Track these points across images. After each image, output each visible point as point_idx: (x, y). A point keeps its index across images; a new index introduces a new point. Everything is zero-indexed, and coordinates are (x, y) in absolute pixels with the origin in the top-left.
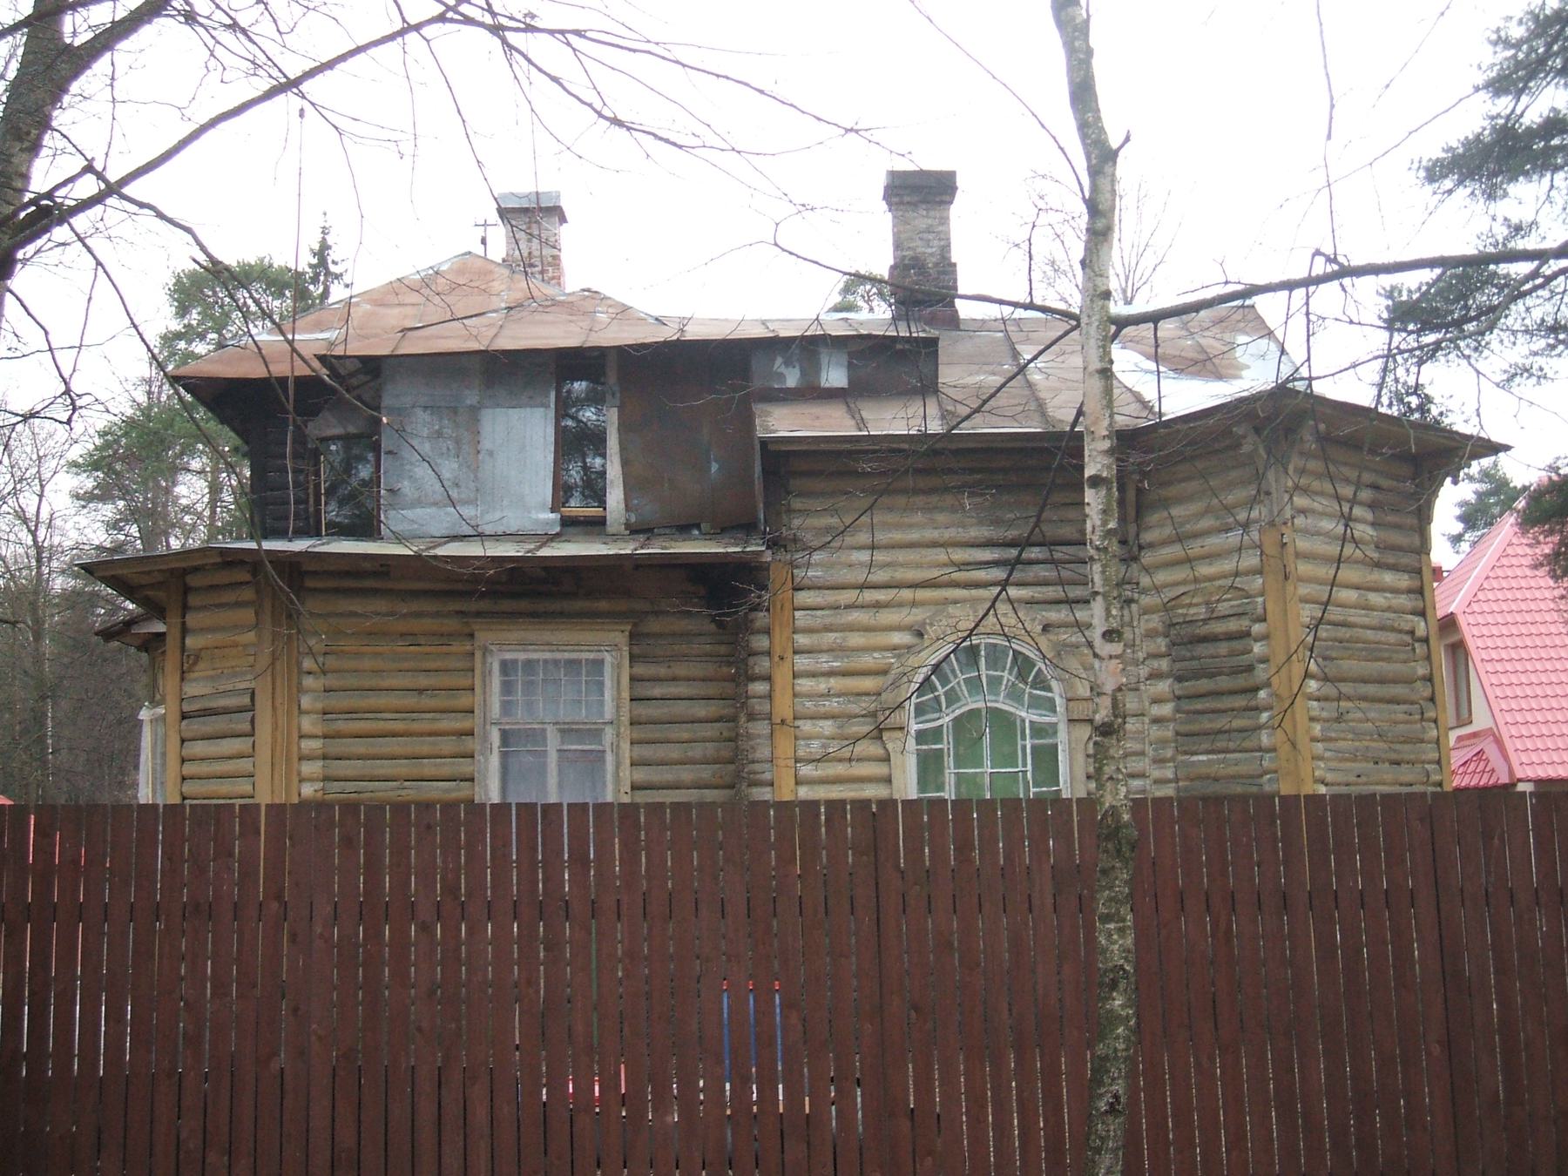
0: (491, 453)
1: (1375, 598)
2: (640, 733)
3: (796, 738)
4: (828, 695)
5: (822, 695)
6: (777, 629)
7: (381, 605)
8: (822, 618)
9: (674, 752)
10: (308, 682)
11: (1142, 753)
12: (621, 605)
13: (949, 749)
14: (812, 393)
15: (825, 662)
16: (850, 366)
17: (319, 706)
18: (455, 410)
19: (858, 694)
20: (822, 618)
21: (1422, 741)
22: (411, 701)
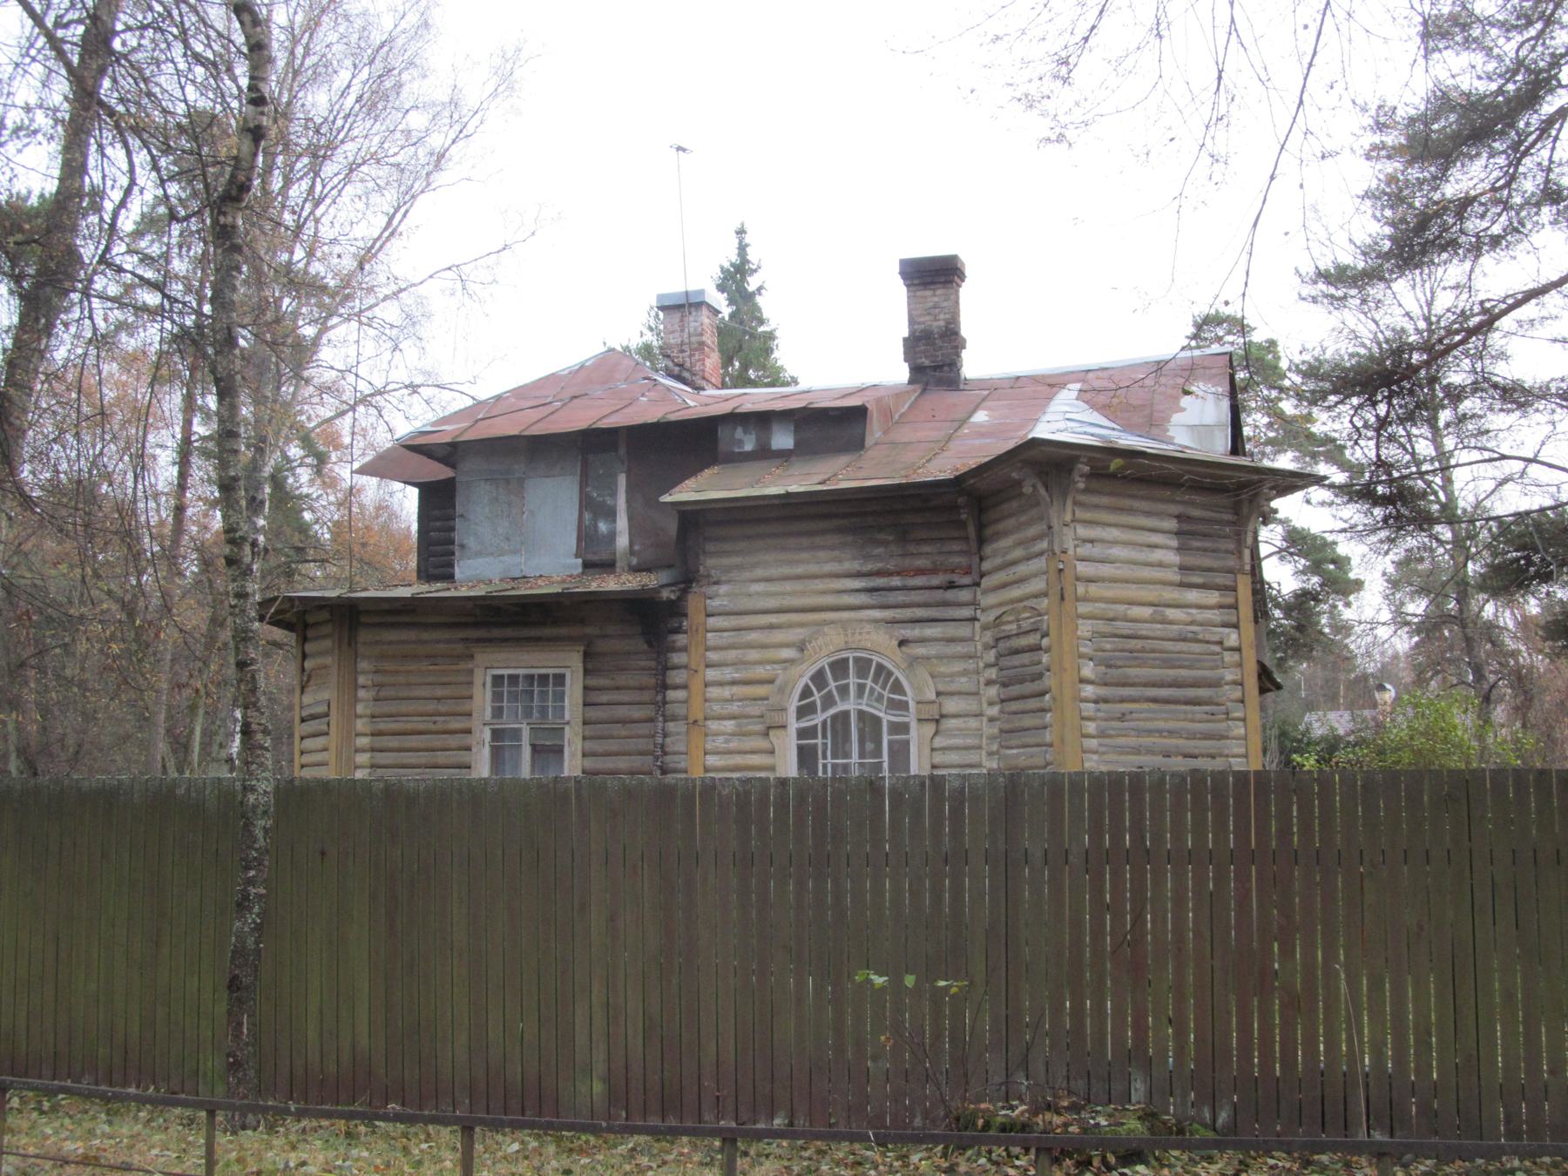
0: (532, 513)
1: (1171, 613)
2: (590, 730)
3: (706, 735)
4: (731, 700)
5: (728, 700)
6: (693, 649)
7: (405, 635)
8: (727, 637)
9: (613, 745)
10: (362, 693)
11: (979, 748)
12: (575, 631)
13: (825, 745)
14: (764, 453)
15: (728, 674)
16: (796, 431)
17: (368, 712)
18: (507, 481)
19: (755, 699)
20: (727, 637)
21: (1227, 738)
22: (431, 707)
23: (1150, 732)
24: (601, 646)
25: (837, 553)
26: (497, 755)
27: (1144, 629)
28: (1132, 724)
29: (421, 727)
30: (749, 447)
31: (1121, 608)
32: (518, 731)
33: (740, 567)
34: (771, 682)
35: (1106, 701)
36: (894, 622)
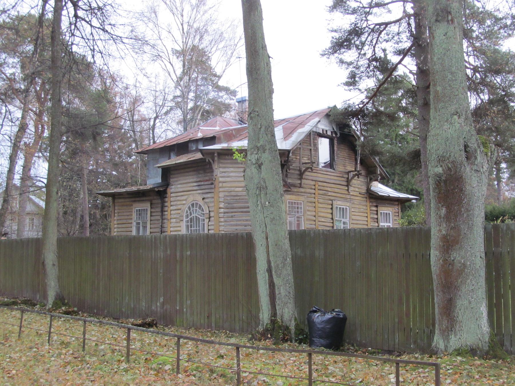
22: (126, 217)
23: (240, 220)
24: (154, 202)
25: (192, 177)
26: (138, 229)
27: (239, 194)
28: (235, 218)
29: (124, 222)
30: (194, 149)
31: (233, 189)
32: (140, 223)
33: (177, 181)
34: (180, 209)
35: (227, 213)
36: (203, 193)
